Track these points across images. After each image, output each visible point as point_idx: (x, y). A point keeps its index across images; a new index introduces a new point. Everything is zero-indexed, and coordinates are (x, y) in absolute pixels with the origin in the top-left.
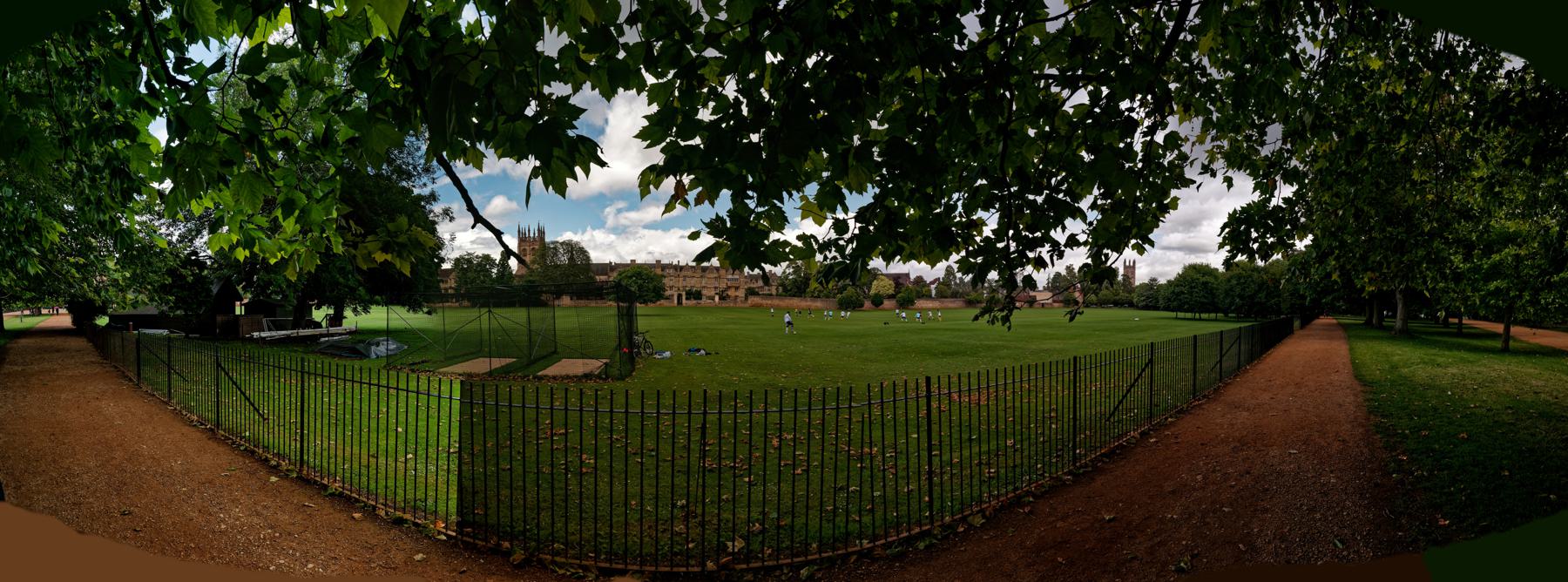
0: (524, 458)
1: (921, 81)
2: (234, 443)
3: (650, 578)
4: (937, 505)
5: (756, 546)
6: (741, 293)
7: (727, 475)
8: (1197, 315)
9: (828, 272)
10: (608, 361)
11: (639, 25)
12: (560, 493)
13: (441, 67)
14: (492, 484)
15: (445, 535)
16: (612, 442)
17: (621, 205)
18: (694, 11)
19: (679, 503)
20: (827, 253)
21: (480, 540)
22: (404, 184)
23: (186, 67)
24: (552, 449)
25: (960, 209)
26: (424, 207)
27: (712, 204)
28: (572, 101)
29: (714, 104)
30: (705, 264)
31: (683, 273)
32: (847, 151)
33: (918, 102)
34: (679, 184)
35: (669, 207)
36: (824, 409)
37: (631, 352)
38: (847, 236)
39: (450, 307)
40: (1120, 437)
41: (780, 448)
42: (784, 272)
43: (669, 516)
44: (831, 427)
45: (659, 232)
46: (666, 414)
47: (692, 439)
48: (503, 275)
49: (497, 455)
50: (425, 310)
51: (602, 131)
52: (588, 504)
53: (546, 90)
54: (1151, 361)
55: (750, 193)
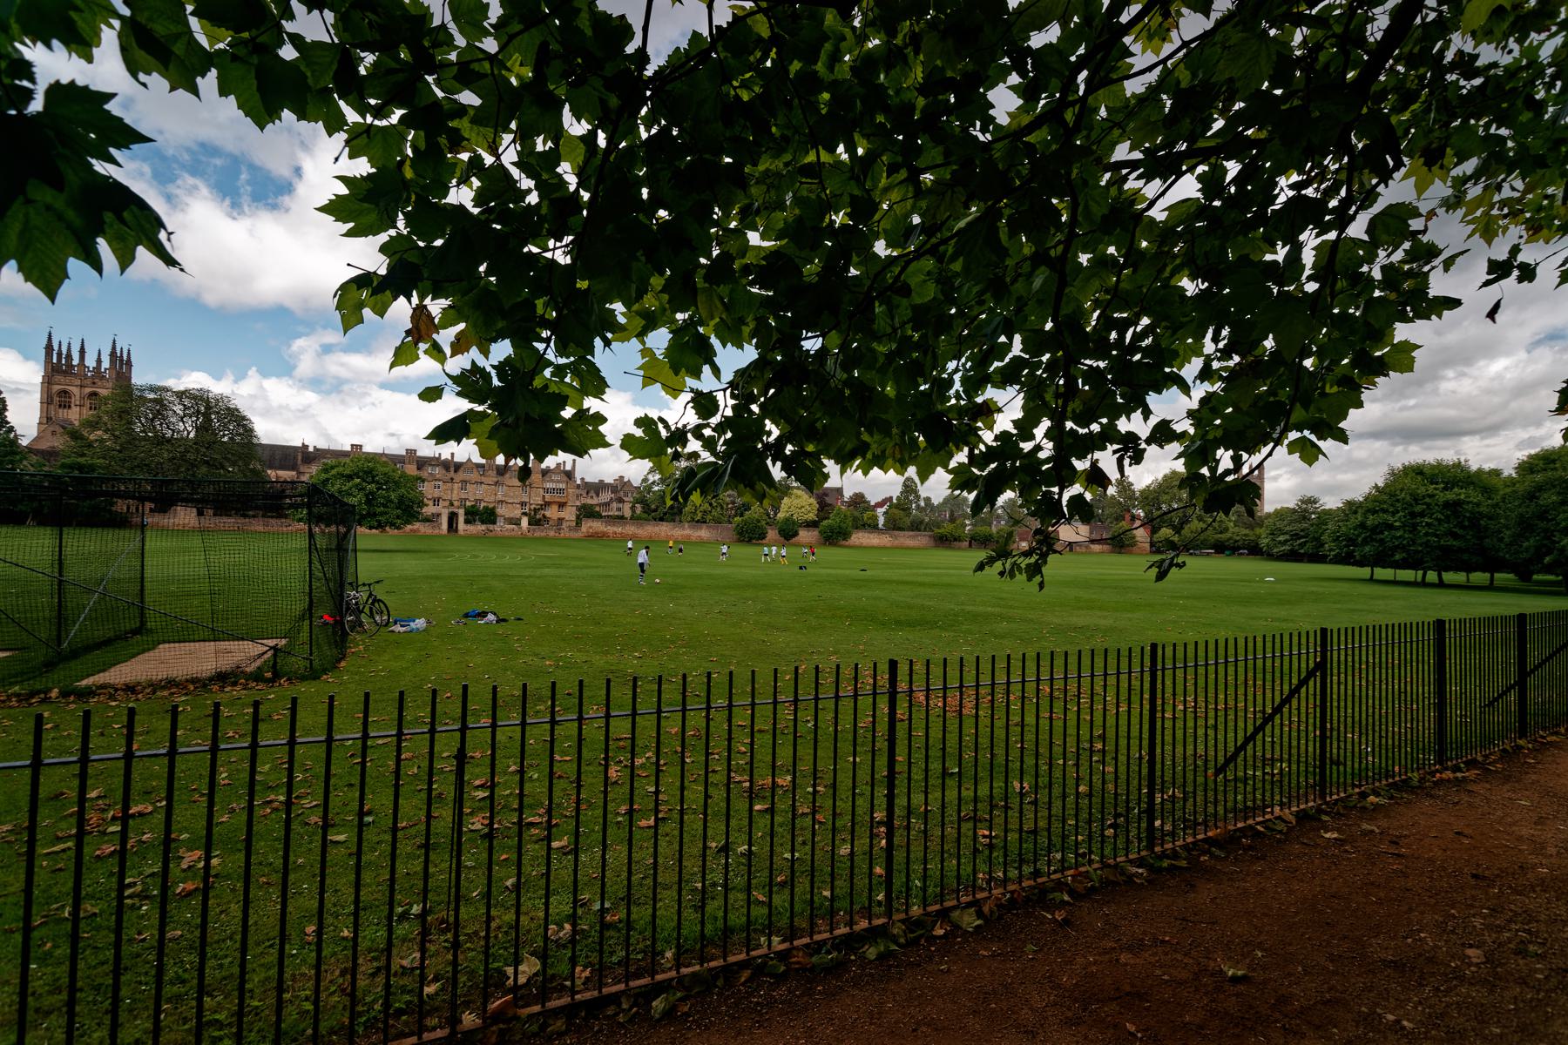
4: (899, 880)
6: (569, 514)
8: (1432, 576)
18: (436, 22)
25: (957, 386)
31: (461, 475)
34: (420, 313)
35: (403, 355)
38: (714, 420)
40: (1247, 812)
42: (645, 480)
54: (1321, 666)
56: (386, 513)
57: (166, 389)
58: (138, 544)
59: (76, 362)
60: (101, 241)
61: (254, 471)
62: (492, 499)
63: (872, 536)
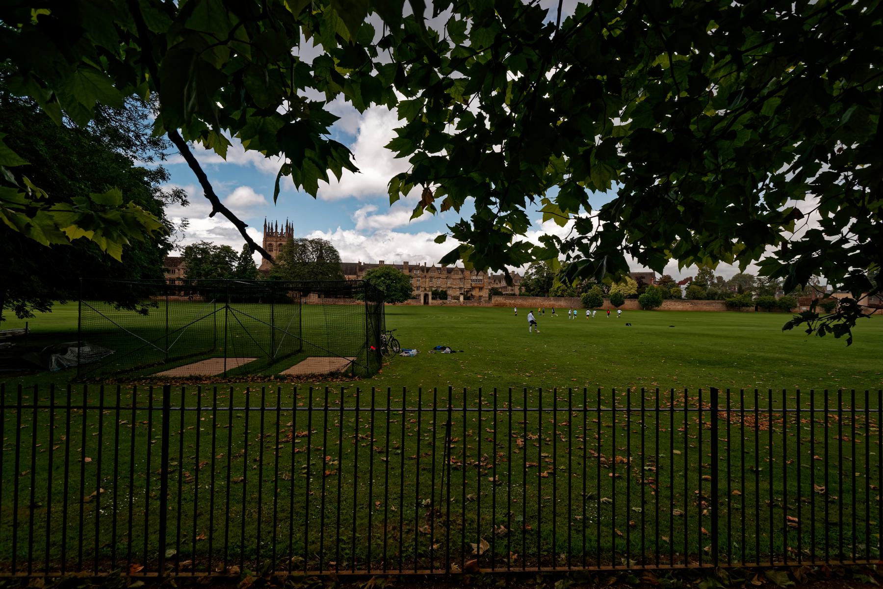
0: (261, 465)
1: (669, 66)
3: (393, 583)
5: (501, 550)
6: (485, 293)
7: (472, 473)
9: (571, 271)
10: (355, 359)
11: (391, 49)
12: (300, 499)
13: (181, 39)
14: (220, 501)
16: (357, 441)
17: (371, 208)
18: (441, 39)
19: (424, 502)
20: (570, 252)
21: (201, 571)
22: (120, 151)
24: (293, 453)
25: (762, 200)
26: (148, 184)
27: (458, 210)
28: (327, 108)
29: (459, 120)
30: (450, 266)
31: (430, 274)
32: (587, 154)
33: (666, 89)
34: (427, 192)
35: (417, 213)
36: (570, 410)
37: (378, 350)
38: (590, 235)
39: (175, 301)
41: (525, 448)
42: (527, 273)
43: (414, 515)
44: (578, 431)
45: (407, 235)
46: (412, 411)
47: (438, 436)
48: (245, 269)
49: (229, 467)
50: (139, 308)
51: (354, 139)
52: (330, 508)
53: (300, 93)
55: (493, 199)
56: (395, 295)
57: (306, 240)
59: (274, 231)
63: (677, 304)
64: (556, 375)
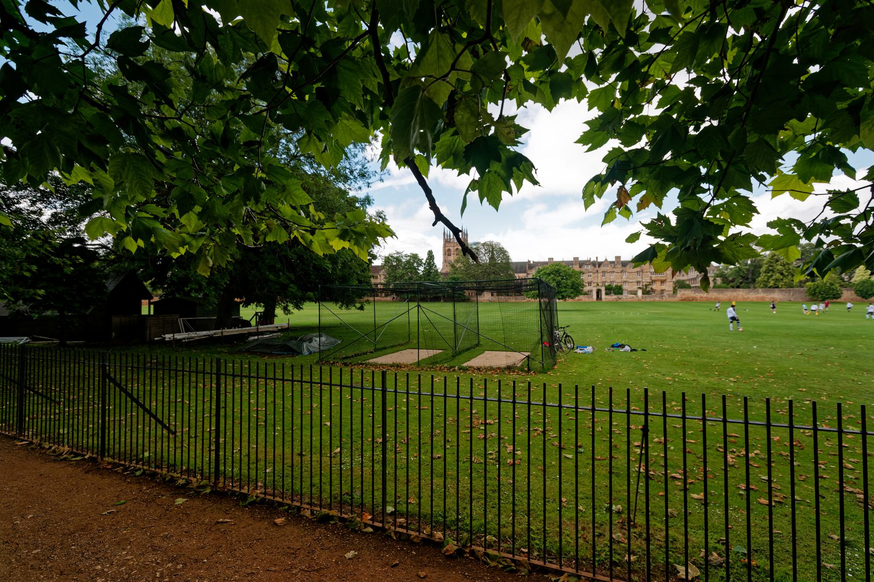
2: (126, 469)
15: (372, 526)
22: (341, 185)
23: (48, 15)
31: (602, 269)
34: (621, 190)
39: (380, 301)
50: (358, 305)
56: (565, 291)
57: (478, 243)
58: (476, 308)
60: (512, 181)
61: (510, 275)
62: (620, 281)
64: (774, 383)
